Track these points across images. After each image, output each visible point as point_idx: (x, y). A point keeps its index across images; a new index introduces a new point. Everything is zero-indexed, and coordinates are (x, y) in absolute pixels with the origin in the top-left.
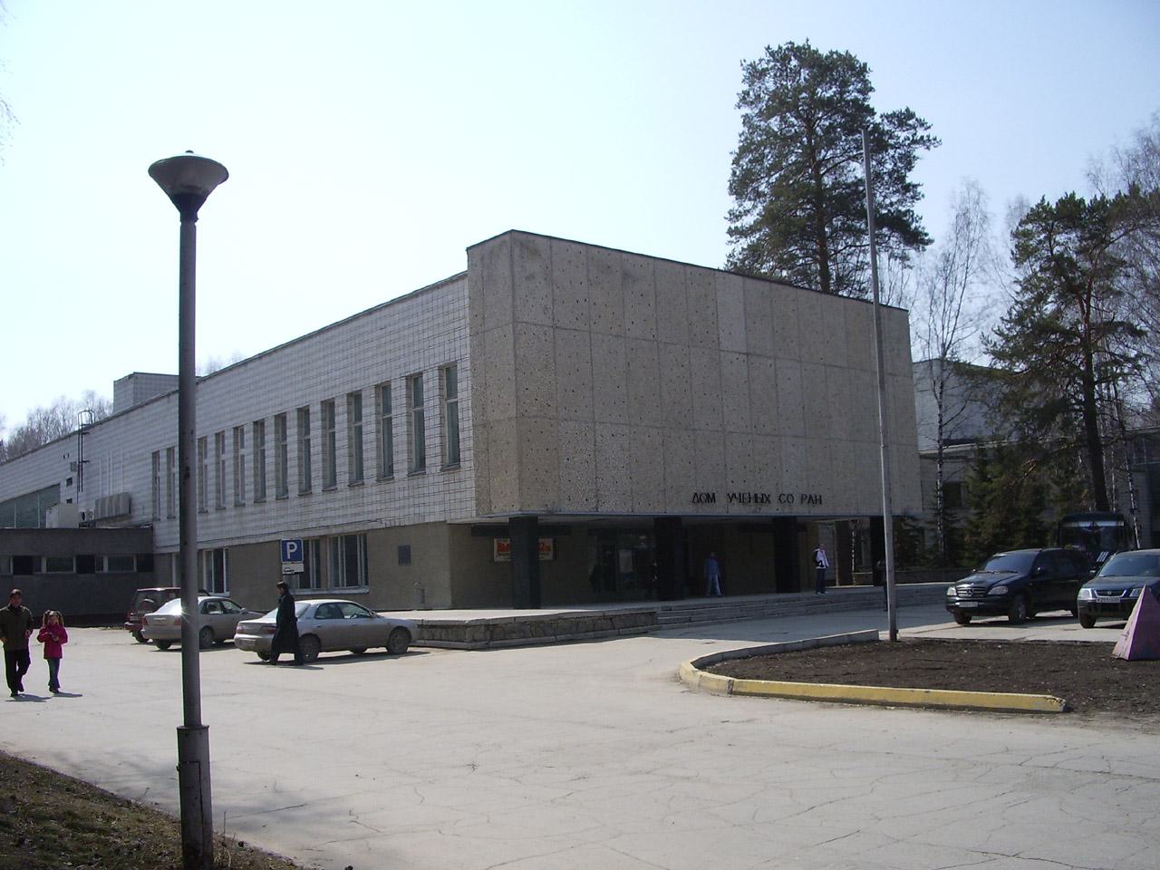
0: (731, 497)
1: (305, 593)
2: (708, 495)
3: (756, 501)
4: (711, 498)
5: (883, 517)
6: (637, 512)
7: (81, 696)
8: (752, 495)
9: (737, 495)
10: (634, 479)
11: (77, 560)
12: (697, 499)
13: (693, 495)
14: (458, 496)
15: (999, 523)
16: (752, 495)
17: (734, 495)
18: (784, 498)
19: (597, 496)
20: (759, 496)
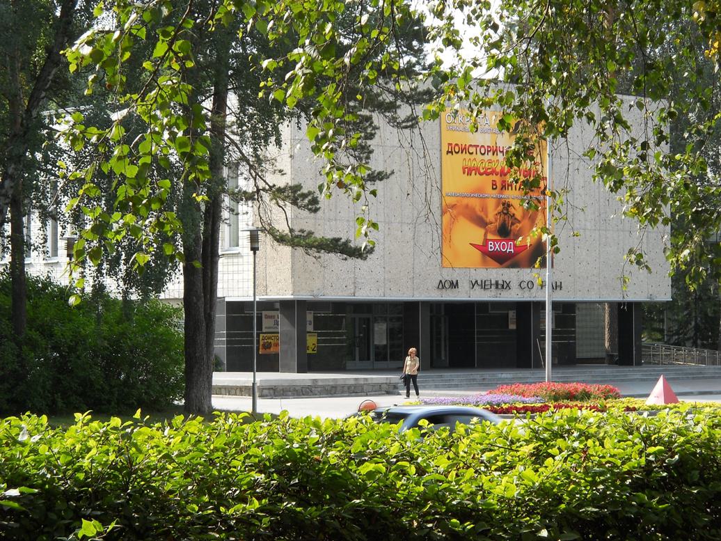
0: (473, 284)
1: (210, 250)
2: (452, 283)
3: (497, 288)
4: (454, 285)
5: (554, 365)
6: (388, 298)
7: (471, 244)
8: (493, 282)
9: (479, 282)
10: (387, 269)
11: (609, 307)
12: (442, 285)
13: (438, 282)
14: (236, 276)
15: (637, 461)
16: (493, 282)
17: (476, 281)
18: (524, 285)
19: (355, 283)
20: (500, 282)
